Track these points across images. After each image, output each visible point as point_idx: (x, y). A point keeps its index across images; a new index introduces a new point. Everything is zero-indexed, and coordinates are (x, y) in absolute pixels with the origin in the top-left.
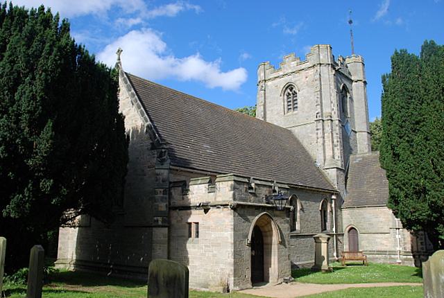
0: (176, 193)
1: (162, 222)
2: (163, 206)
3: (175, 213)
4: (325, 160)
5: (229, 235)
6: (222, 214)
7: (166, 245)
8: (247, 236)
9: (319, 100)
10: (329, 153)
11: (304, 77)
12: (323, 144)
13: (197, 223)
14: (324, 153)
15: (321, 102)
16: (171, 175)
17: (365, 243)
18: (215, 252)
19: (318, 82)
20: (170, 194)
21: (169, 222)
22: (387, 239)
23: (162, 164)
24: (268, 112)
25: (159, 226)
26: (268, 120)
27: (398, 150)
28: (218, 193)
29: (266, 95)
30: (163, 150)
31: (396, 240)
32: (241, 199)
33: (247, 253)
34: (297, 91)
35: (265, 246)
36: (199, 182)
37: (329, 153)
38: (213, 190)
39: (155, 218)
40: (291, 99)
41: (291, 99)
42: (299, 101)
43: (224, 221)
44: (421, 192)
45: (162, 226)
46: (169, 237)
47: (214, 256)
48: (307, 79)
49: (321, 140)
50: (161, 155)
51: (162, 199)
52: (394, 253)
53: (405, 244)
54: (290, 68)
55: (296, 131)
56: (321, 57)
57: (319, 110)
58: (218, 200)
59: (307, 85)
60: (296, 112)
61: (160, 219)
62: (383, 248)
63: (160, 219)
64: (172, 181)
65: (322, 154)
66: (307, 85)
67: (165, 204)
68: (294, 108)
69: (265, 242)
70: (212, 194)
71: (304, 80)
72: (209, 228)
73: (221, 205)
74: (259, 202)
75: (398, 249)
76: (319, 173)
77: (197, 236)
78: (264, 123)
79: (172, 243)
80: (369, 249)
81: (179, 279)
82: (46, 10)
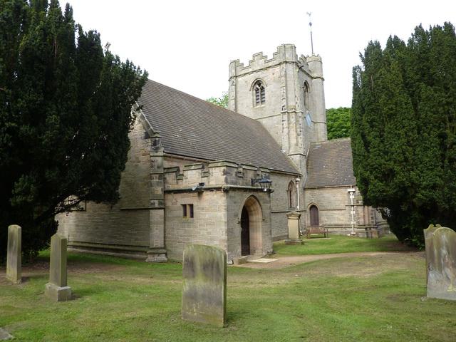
0: (171, 178)
1: (159, 204)
2: (159, 190)
3: (170, 197)
4: (289, 147)
5: (222, 215)
6: (215, 196)
7: (163, 226)
8: (237, 215)
9: (285, 95)
10: (293, 141)
11: (271, 74)
12: (288, 134)
13: (191, 206)
14: (291, 143)
15: (287, 97)
16: (165, 162)
17: (325, 218)
18: (209, 230)
19: (283, 78)
20: (165, 179)
21: (165, 204)
22: (343, 215)
23: (157, 152)
24: (239, 106)
25: (156, 209)
26: (239, 112)
27: (369, 138)
28: (211, 178)
29: (238, 90)
30: (157, 139)
31: (351, 216)
32: (232, 183)
33: (238, 229)
34: (265, 86)
35: (250, 224)
36: (193, 167)
37: (293, 141)
38: (206, 175)
39: (152, 201)
40: (259, 94)
41: (259, 94)
42: (266, 95)
43: (217, 203)
44: (388, 175)
45: (159, 209)
46: (165, 217)
47: (209, 233)
48: (274, 75)
49: (286, 131)
50: (155, 144)
51: (158, 184)
52: (348, 226)
53: (359, 218)
54: (258, 65)
55: (264, 122)
56: (287, 56)
57: (285, 104)
58: (211, 183)
59: (274, 81)
60: (263, 105)
61: (156, 202)
62: (340, 223)
63: (156, 202)
64: (165, 167)
65: (287, 143)
66: (274, 81)
67: (161, 188)
68: (262, 102)
69: (250, 219)
70: (206, 178)
71: (271, 76)
72: (203, 209)
73: (215, 188)
74: (247, 184)
75: (352, 223)
76: (284, 159)
77: (192, 216)
78: (235, 113)
79: (167, 223)
80: (328, 223)
81: (218, 263)
82: (393, 37)
